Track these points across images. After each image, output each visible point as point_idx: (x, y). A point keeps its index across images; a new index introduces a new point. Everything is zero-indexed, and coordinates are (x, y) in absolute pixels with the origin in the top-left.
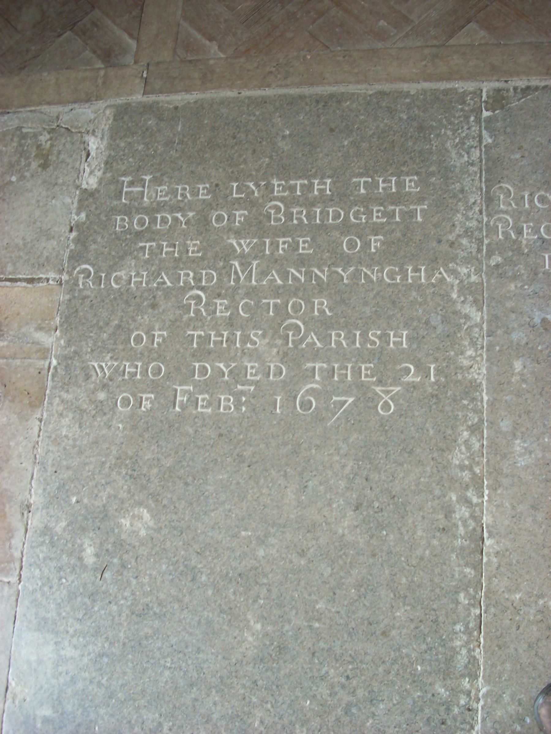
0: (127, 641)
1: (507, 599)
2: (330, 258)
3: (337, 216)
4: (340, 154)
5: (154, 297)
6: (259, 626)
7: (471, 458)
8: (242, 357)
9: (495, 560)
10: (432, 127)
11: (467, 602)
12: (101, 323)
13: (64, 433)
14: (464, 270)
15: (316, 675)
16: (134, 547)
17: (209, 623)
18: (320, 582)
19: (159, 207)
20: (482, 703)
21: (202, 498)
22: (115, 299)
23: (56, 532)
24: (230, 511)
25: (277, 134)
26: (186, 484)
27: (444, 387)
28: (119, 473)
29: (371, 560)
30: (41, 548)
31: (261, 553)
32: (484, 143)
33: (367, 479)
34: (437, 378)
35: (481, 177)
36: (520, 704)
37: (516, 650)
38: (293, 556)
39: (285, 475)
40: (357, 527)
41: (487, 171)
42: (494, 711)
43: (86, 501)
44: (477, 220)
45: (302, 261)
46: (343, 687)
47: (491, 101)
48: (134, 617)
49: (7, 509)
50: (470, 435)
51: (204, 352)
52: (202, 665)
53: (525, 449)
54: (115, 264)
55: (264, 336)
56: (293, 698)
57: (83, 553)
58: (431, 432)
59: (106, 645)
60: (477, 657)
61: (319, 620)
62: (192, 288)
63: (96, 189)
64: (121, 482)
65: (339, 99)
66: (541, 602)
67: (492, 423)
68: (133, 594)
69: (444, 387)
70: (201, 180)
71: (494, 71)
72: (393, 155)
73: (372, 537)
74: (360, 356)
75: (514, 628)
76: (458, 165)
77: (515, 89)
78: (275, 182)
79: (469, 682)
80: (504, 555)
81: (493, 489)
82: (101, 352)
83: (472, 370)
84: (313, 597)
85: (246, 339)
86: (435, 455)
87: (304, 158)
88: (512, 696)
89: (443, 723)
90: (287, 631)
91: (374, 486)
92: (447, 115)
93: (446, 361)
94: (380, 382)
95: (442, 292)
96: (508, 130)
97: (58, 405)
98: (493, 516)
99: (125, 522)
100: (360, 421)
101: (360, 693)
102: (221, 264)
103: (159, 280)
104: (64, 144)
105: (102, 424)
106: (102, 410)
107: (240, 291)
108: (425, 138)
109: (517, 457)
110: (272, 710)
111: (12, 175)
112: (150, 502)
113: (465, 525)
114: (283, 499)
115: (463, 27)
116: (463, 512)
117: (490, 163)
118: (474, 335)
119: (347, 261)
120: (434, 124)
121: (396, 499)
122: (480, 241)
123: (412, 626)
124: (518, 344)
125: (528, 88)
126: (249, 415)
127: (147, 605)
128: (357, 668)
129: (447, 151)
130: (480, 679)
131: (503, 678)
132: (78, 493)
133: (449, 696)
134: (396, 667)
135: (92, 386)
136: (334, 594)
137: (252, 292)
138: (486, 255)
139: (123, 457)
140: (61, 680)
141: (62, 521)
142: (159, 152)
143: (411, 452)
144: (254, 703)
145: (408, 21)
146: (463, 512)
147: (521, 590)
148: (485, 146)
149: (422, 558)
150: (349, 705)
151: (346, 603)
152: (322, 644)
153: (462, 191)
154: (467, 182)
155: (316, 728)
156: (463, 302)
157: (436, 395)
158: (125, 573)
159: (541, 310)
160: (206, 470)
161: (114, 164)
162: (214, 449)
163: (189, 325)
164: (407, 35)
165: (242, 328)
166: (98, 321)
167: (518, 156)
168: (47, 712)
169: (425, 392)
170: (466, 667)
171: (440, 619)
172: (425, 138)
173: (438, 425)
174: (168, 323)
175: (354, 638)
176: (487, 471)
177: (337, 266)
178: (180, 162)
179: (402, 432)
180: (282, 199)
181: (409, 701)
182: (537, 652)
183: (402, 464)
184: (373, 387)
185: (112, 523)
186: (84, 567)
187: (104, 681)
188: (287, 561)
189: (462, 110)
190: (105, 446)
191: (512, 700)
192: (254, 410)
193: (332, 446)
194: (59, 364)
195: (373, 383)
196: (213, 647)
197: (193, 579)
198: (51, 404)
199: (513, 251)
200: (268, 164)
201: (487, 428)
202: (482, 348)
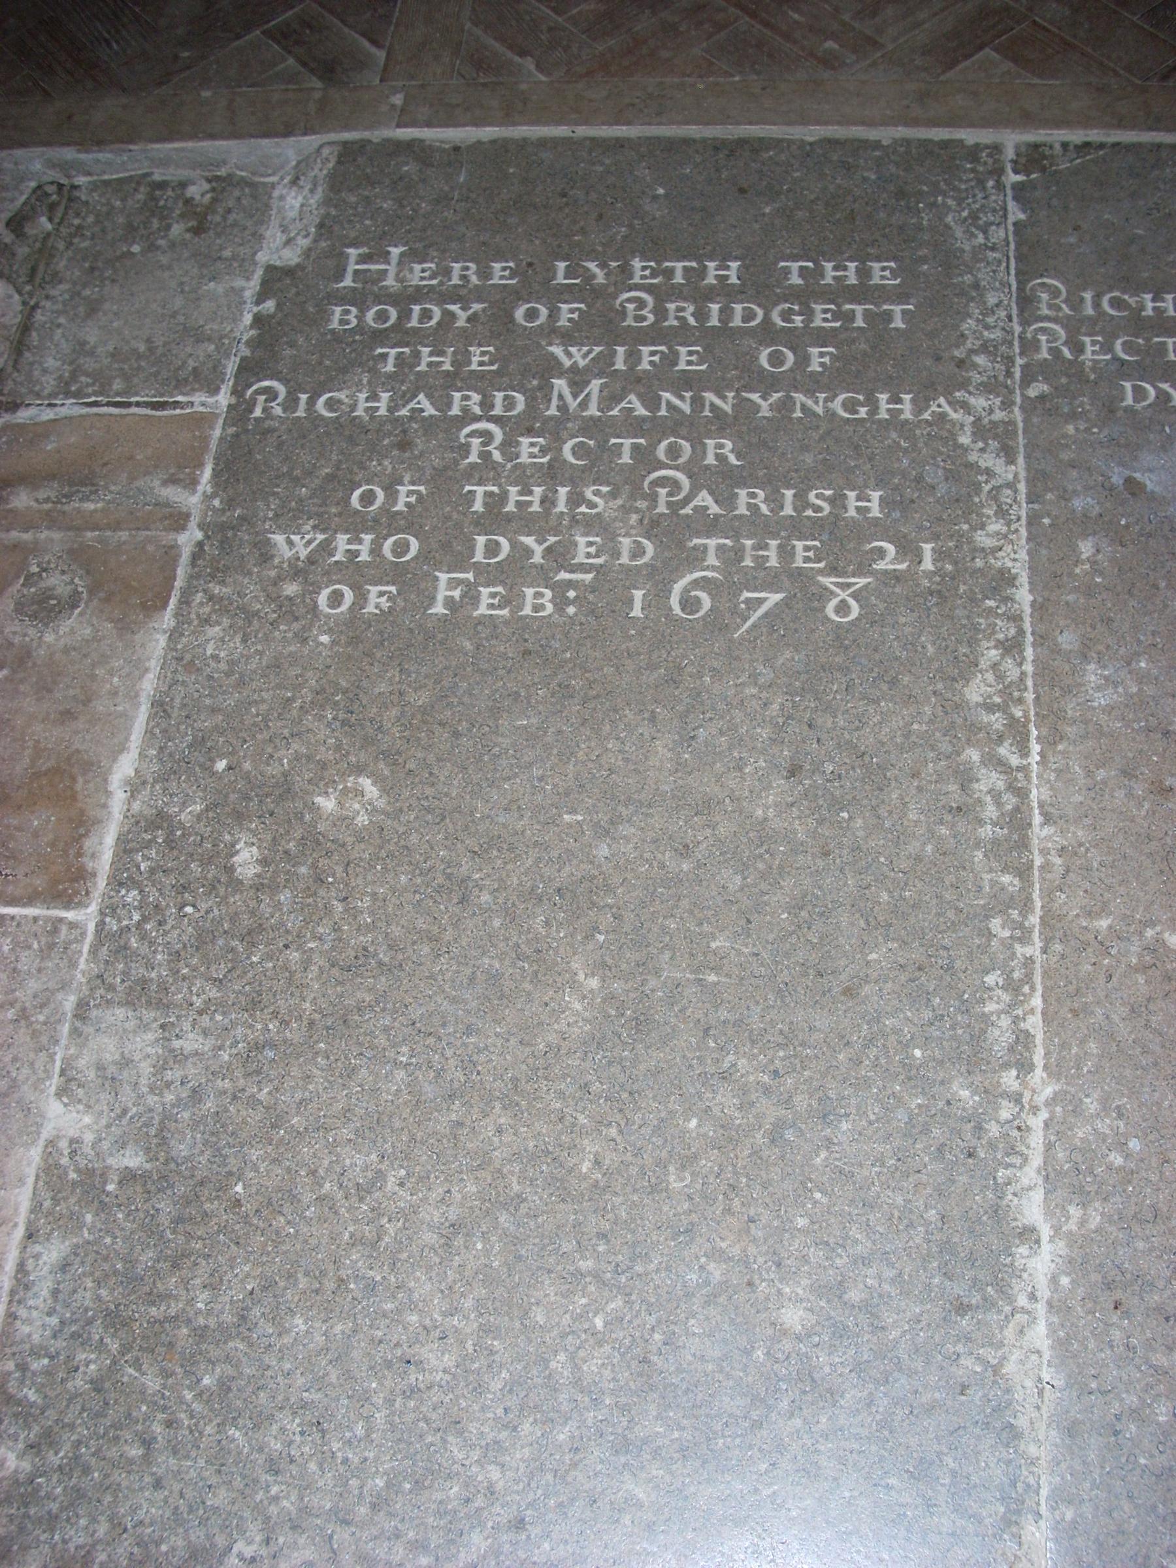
0: (317, 1016)
2: (739, 378)
3: (749, 316)
4: (756, 226)
5: (404, 432)
6: (594, 983)
7: (1006, 692)
8: (571, 527)
9: (1058, 861)
10: (921, 193)
11: (1006, 933)
12: (297, 472)
13: (209, 653)
14: (979, 402)
15: (710, 1069)
16: (343, 845)
17: (494, 978)
18: (719, 900)
19: (419, 294)
20: (1044, 1115)
21: (486, 758)
22: (327, 434)
23: (180, 822)
24: (541, 779)
25: (644, 193)
26: (456, 734)
27: (953, 578)
28: (321, 718)
29: (820, 863)
30: (146, 852)
31: (603, 851)
32: (1011, 219)
33: (810, 726)
35: (1008, 267)
36: (1120, 1116)
37: (1107, 1017)
38: (667, 854)
39: (653, 719)
40: (792, 805)
41: (1019, 259)
43: (247, 766)
44: (1003, 329)
45: (686, 382)
46: (767, 1091)
47: (1023, 160)
48: (335, 971)
49: (79, 786)
50: (1003, 656)
51: (495, 517)
52: (475, 1058)
53: (1106, 678)
54: (331, 379)
55: (613, 495)
56: (663, 1115)
57: (235, 859)
58: (931, 650)
59: (271, 1026)
60: (1031, 1031)
61: (715, 969)
62: (478, 419)
63: (298, 265)
64: (323, 732)
65: (755, 146)
66: (1149, 933)
68: (336, 929)
69: (953, 578)
70: (500, 256)
71: (1027, 119)
72: (852, 231)
73: (821, 822)
74: (797, 528)
75: (1102, 978)
76: (967, 248)
77: (1065, 145)
78: (637, 264)
79: (1018, 1077)
81: (1050, 742)
82: (295, 518)
83: (1001, 554)
84: (706, 928)
85: (576, 499)
86: (940, 686)
87: (691, 229)
88: (1105, 1102)
89: (970, 1155)
90: (653, 991)
91: (824, 736)
94: (833, 570)
95: (945, 434)
96: (1055, 202)
97: (201, 604)
98: (1051, 789)
99: (327, 804)
100: (796, 631)
101: (801, 1101)
102: (535, 382)
103: (412, 405)
104: (239, 199)
105: (290, 635)
106: (292, 612)
107: (570, 425)
108: (908, 208)
110: (619, 1139)
111: (134, 242)
112: (381, 765)
113: (999, 804)
114: (646, 758)
115: (971, 56)
116: (997, 780)
117: (1025, 249)
118: (1003, 499)
119: (768, 383)
121: (867, 759)
122: (1009, 361)
123: (903, 978)
124: (1085, 515)
125: (1087, 144)
126: (583, 620)
127: (365, 949)
128: (795, 1056)
129: (948, 227)
130: (1039, 1072)
132: (233, 753)
133: (980, 1104)
134: (873, 1052)
135: (273, 573)
136: (749, 922)
137: (591, 427)
138: (1022, 381)
139: (330, 690)
140: (170, 1097)
141: (195, 803)
142: (422, 212)
143: (894, 682)
144: (583, 1126)
145: (875, 44)
146: (989, 780)
147: (1111, 913)
148: (1015, 224)
149: (919, 859)
150: (779, 1126)
151: (771, 937)
152: (723, 1014)
153: (976, 286)
154: (984, 275)
155: (712, 1172)
156: (982, 450)
157: (939, 592)
158: (322, 892)
159: (1122, 464)
160: (495, 712)
161: (336, 228)
162: (513, 675)
163: (471, 475)
164: (874, 64)
165: (572, 482)
166: (292, 469)
168: (133, 1159)
169: (918, 585)
170: (1011, 1049)
171: (958, 964)
172: (908, 208)
174: (429, 472)
175: (788, 999)
176: (1037, 714)
177: (752, 390)
178: (462, 229)
179: (875, 650)
180: (649, 289)
181: (901, 1115)
183: (877, 702)
184: (820, 578)
185: (299, 804)
186: (236, 884)
187: (263, 1095)
188: (655, 864)
189: (973, 170)
190: (294, 672)
191: (1104, 1109)
192: (593, 611)
193: (744, 671)
194: (208, 537)
195: (821, 572)
196: (498, 1022)
197: (463, 900)
198: (185, 601)
199: (1068, 376)
200: (625, 237)
201: (1034, 645)
202: (1019, 519)
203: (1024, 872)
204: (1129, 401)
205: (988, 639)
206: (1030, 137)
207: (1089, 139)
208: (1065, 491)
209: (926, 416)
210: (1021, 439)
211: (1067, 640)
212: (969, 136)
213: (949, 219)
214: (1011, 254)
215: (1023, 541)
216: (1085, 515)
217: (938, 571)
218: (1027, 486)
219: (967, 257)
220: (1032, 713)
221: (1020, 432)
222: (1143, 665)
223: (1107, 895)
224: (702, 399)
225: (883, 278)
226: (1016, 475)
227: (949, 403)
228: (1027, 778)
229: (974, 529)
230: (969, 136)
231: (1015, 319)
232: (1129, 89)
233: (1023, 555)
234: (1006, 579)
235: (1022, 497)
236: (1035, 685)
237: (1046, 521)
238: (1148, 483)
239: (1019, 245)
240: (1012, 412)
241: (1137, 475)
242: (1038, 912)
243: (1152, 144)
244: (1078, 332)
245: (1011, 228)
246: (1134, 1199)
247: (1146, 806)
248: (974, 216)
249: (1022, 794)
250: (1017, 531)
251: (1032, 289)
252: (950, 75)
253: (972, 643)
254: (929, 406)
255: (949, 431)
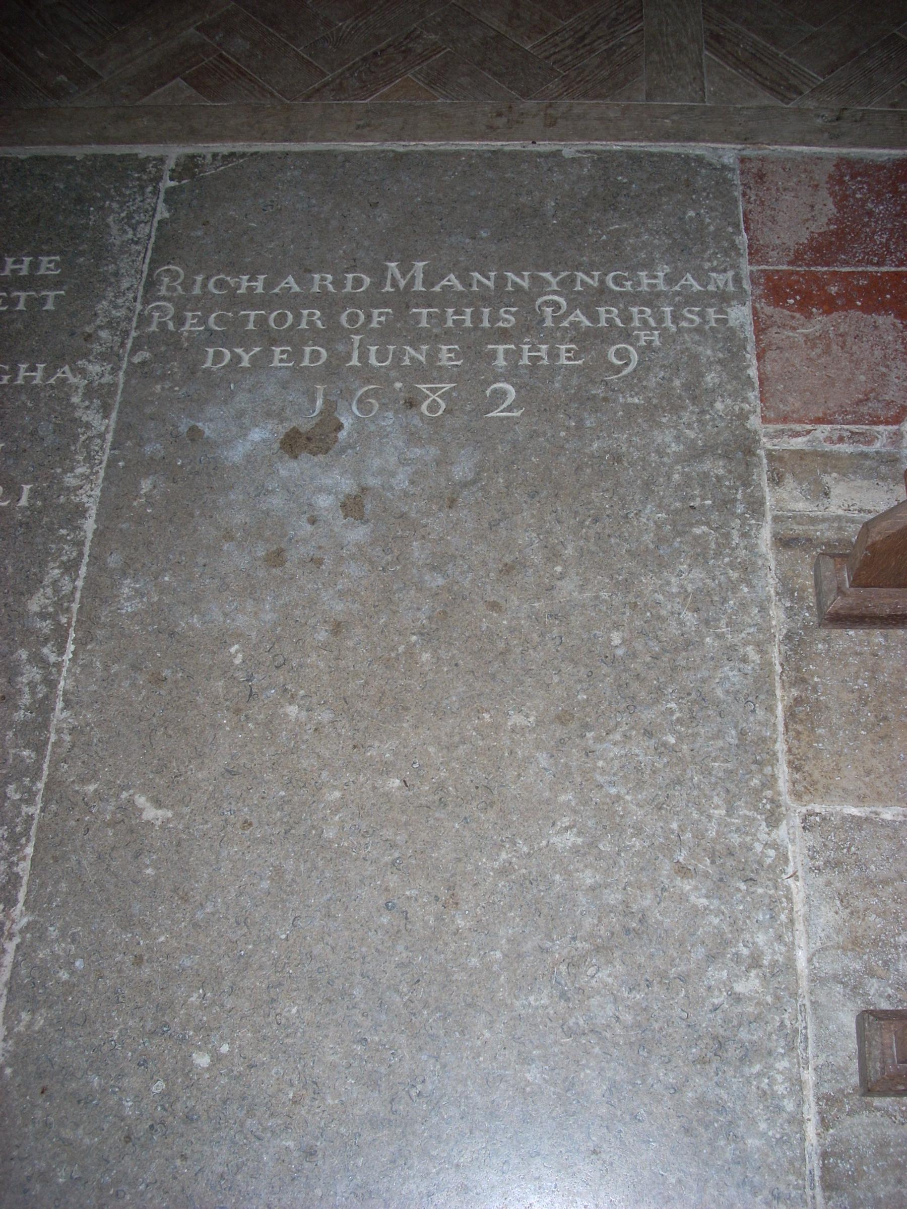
1: (77, 791)
7: (58, 605)
9: (68, 738)
11: (18, 797)
14: (94, 369)
20: (17, 940)
27: (40, 512)
34: (32, 501)
35: (144, 258)
37: (79, 863)
42: (35, 951)
44: (128, 308)
50: (62, 574)
53: (136, 590)
60: (21, 873)
66: (124, 795)
67: (95, 558)
72: (35, 232)
75: (82, 831)
77: (215, 156)
80: (82, 732)
81: (80, 643)
83: (81, 491)
92: (117, 185)
93: (49, 480)
95: (62, 395)
96: (195, 202)
108: (82, 211)
109: (122, 601)
113: (33, 693)
115: (163, 84)
116: (32, 673)
120: (99, 195)
122: (126, 333)
125: (232, 154)
129: (108, 226)
130: (20, 906)
131: (54, 904)
138: (131, 350)
146: (32, 673)
153: (116, 274)
156: (87, 408)
167: (199, 233)
173: (22, 561)
176: (78, 620)
177: (547, 270)
182: (109, 865)
201: (88, 564)
203: (39, 748)
204: (208, 364)
205: (54, 561)
206: (190, 150)
207: (234, 150)
208: (142, 439)
209: (52, 381)
210: (118, 398)
211: (114, 561)
212: (142, 151)
213: (110, 220)
214: (150, 247)
215: (100, 481)
216: (152, 458)
217: (31, 507)
218: (114, 437)
219: (115, 250)
220: (74, 619)
221: (119, 392)
222: (166, 579)
223: (99, 765)
224: (505, 278)
225: (48, 269)
226: (107, 427)
227: (72, 370)
228: (59, 672)
229: (65, 472)
230: (142, 151)
231: (139, 299)
232: (279, 107)
233: (97, 492)
234: (80, 511)
235: (108, 445)
236: (82, 597)
237: (121, 464)
238: (206, 430)
239: (158, 238)
240: (117, 376)
241: (200, 424)
242: (44, 778)
243: (282, 153)
244: (184, 309)
245: (155, 225)
246: (71, 1007)
247: (144, 693)
248: (130, 217)
249: (52, 684)
250: (97, 472)
251: (158, 275)
252: (145, 100)
253: (42, 565)
254: (56, 373)
255: (66, 393)
